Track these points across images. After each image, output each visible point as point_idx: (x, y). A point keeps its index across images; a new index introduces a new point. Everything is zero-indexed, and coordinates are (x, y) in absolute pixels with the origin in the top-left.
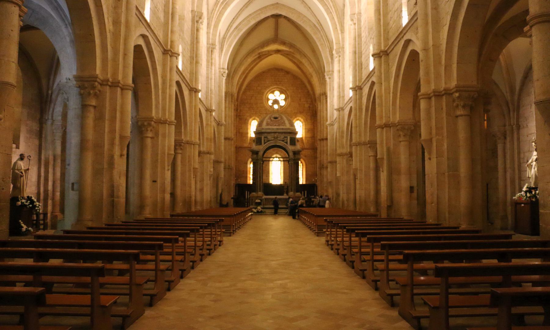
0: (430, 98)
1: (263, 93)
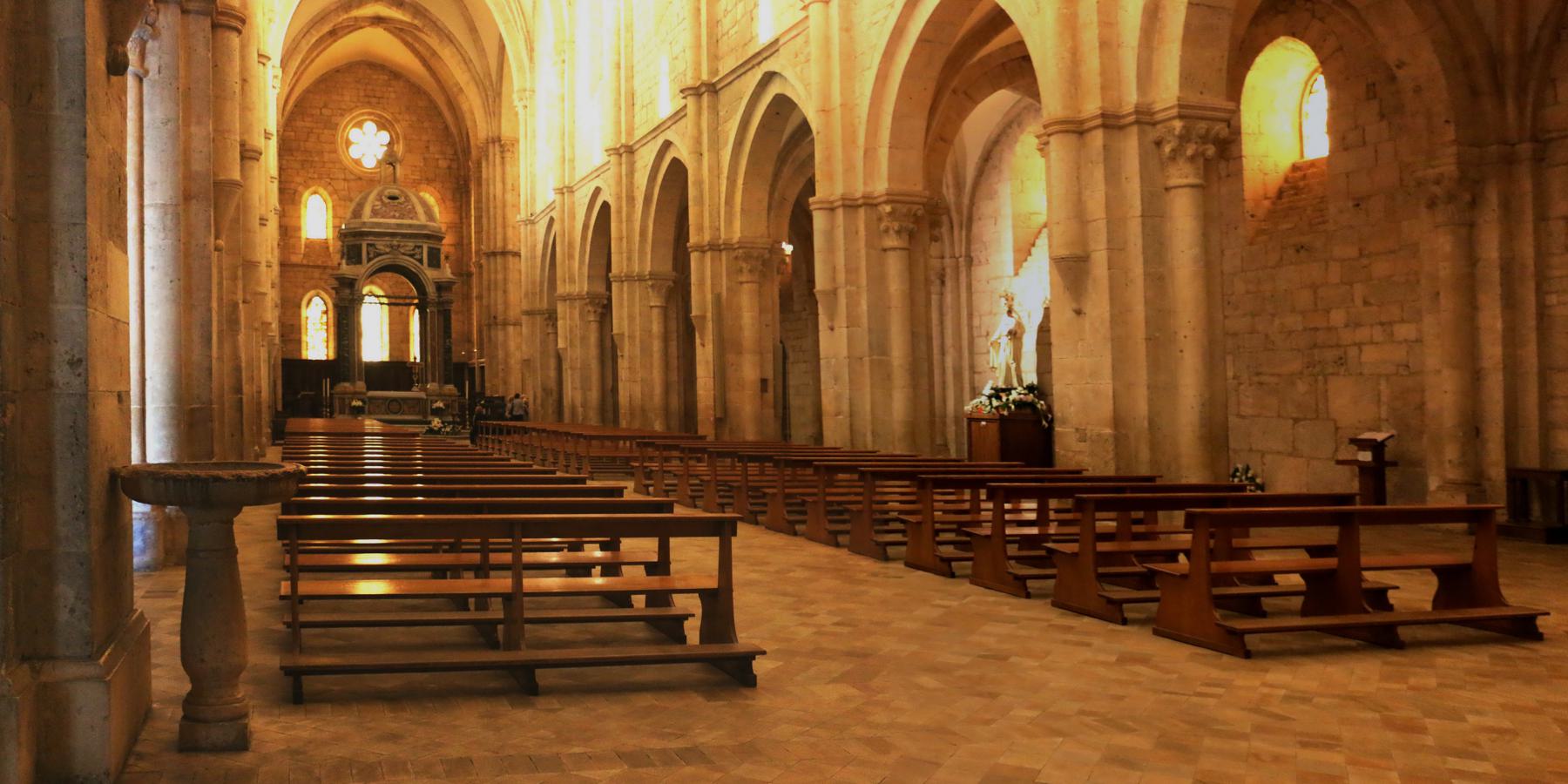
0: (832, 210)
1: (335, 127)
